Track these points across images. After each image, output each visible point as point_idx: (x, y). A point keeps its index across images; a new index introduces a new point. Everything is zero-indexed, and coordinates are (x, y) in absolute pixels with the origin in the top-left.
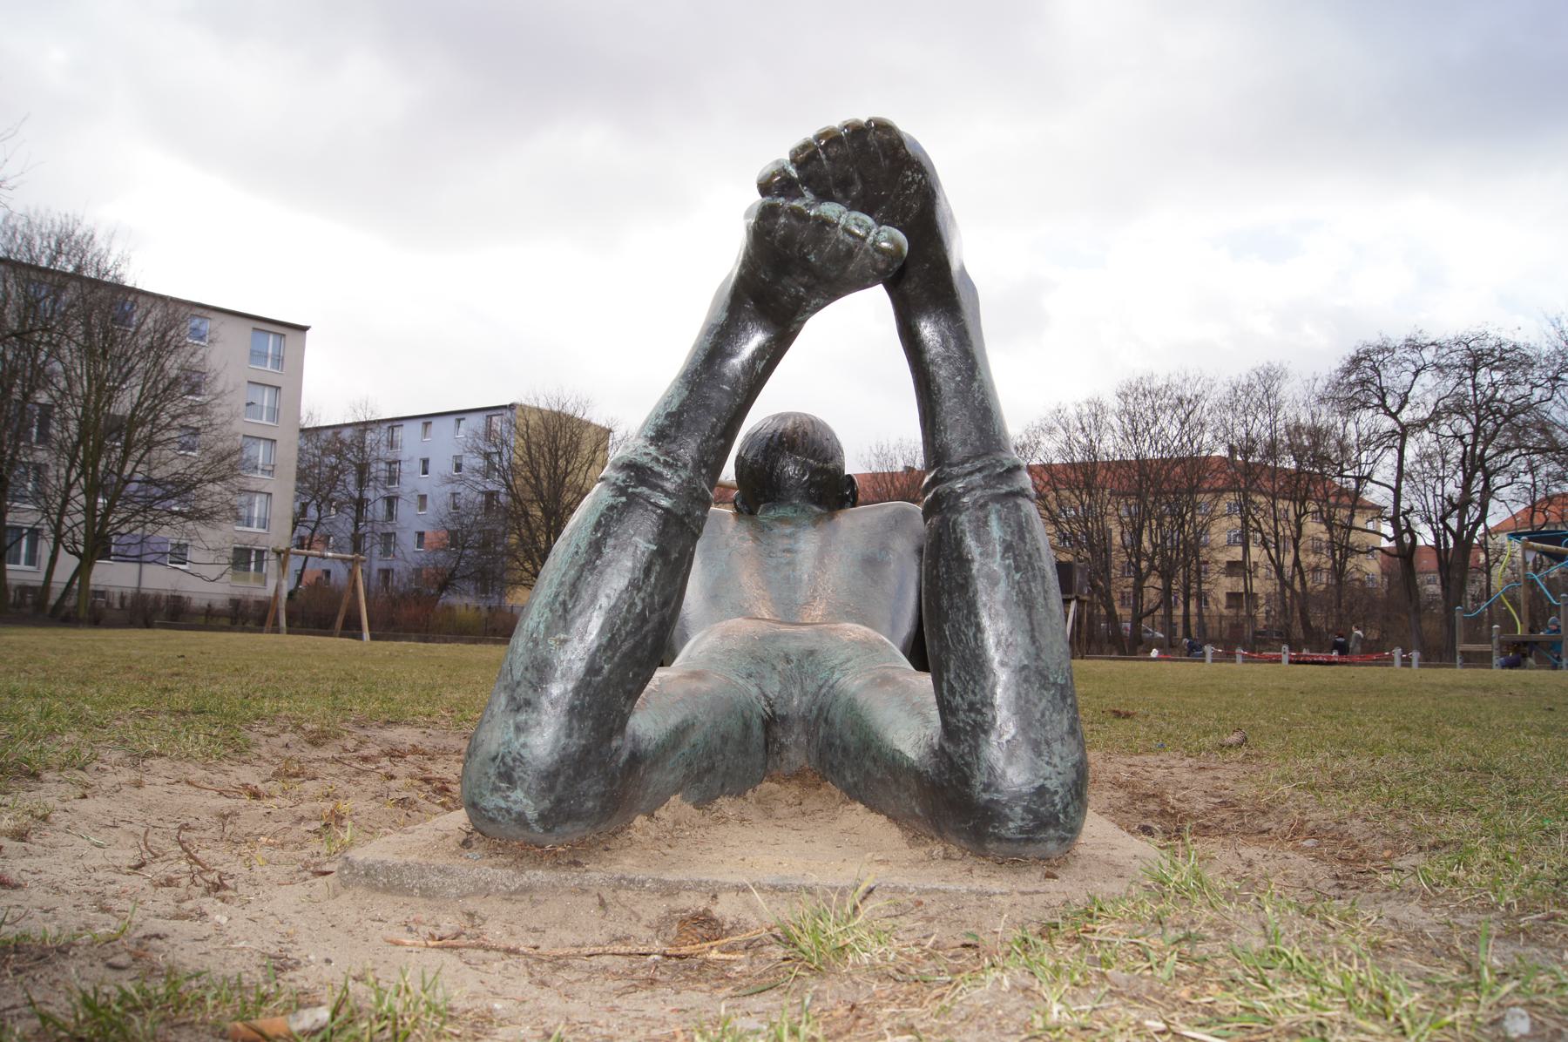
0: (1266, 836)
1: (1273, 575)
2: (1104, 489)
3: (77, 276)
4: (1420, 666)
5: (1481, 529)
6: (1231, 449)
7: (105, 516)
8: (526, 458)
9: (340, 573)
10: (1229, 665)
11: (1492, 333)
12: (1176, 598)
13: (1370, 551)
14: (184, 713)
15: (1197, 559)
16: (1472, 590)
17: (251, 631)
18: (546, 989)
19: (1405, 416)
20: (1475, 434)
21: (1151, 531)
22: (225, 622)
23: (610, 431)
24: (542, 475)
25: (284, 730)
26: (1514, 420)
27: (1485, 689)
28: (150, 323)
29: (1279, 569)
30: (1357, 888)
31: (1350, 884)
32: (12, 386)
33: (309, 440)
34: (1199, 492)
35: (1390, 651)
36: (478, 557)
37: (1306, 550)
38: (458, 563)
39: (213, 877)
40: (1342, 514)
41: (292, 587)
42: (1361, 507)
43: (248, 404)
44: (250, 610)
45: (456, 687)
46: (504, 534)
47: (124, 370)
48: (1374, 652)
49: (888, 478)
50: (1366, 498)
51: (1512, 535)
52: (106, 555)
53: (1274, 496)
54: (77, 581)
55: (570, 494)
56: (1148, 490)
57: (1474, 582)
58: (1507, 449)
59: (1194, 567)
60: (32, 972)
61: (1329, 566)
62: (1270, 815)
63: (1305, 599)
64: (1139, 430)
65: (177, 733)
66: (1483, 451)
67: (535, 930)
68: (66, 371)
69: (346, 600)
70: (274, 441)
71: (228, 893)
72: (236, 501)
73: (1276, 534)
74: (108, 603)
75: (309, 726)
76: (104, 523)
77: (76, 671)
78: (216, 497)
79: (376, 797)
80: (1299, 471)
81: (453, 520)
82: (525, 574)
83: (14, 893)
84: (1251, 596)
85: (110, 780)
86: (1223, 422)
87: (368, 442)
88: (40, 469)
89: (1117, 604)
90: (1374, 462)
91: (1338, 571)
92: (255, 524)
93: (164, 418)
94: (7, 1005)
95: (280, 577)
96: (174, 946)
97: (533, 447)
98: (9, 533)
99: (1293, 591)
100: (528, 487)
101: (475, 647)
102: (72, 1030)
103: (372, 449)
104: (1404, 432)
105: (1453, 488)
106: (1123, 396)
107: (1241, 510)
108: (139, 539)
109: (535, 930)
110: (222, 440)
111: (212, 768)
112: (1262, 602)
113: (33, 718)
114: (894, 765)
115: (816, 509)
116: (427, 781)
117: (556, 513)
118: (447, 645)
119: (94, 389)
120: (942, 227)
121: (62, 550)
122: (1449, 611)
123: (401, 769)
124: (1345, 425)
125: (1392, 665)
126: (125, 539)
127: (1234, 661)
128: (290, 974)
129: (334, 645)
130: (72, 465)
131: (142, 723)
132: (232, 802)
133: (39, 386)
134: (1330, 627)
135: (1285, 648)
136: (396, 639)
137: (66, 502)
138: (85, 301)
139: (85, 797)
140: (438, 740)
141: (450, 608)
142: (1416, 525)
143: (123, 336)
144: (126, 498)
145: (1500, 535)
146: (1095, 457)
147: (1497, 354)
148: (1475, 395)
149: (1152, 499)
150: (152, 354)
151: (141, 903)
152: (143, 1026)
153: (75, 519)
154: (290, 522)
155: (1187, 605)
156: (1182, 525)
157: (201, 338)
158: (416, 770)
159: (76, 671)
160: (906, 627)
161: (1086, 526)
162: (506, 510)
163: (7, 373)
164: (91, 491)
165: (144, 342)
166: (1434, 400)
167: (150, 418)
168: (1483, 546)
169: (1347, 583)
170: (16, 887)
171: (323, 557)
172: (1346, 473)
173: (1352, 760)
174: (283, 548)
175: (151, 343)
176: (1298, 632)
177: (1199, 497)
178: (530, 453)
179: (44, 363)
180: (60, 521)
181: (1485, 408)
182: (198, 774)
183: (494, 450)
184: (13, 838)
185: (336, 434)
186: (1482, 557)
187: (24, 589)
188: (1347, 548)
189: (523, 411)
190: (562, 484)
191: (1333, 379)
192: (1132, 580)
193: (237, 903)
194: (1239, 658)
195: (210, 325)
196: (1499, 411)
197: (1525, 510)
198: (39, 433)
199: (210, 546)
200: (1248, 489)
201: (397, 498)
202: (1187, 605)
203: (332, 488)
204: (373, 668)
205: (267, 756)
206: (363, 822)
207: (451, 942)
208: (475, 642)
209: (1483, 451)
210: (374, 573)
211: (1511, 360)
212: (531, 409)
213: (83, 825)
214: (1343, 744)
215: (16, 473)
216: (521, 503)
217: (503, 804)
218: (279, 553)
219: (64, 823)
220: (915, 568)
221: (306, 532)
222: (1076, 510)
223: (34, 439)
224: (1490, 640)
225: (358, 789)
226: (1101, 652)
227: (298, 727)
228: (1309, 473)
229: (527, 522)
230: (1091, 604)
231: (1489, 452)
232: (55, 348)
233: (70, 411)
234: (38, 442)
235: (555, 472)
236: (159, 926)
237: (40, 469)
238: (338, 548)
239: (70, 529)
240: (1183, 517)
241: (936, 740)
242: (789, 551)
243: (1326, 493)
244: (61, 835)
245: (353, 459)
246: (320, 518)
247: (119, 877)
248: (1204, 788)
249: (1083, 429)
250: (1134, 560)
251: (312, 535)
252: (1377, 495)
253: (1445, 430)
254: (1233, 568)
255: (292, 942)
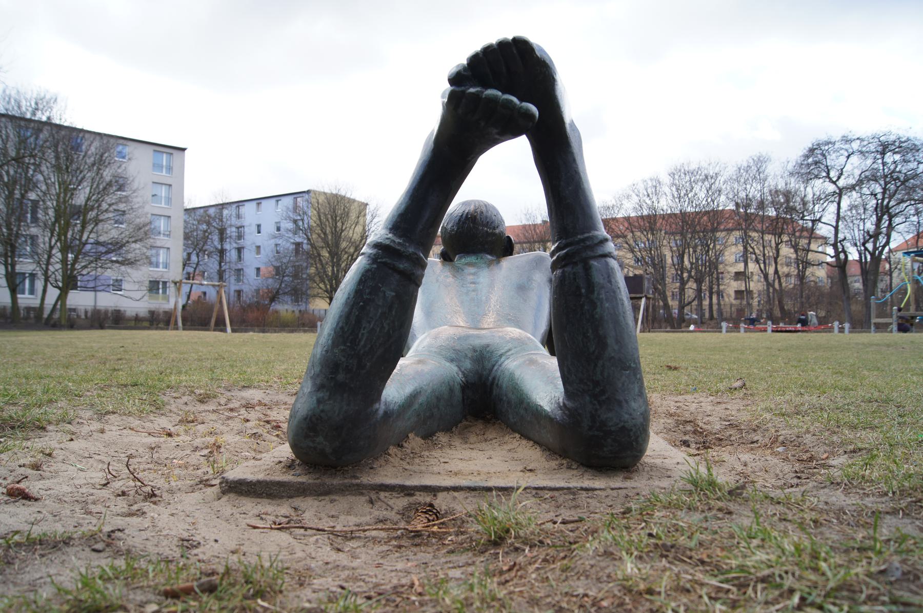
0: (755, 445)
1: (762, 280)
2: (661, 231)
3: (49, 123)
4: (850, 332)
5: (887, 249)
6: (737, 205)
7: (73, 265)
8: (318, 222)
9: (212, 294)
10: (736, 334)
11: (894, 131)
12: (705, 294)
13: (820, 264)
14: (126, 386)
15: (717, 271)
16: (881, 285)
17: (162, 329)
18: (341, 553)
19: (841, 183)
20: (884, 193)
21: (689, 255)
22: (146, 324)
23: (367, 204)
24: (328, 232)
25: (184, 394)
26: (907, 184)
27: (888, 346)
28: (93, 149)
29: (766, 276)
30: (808, 478)
31: (803, 476)
32: (14, 190)
33: (190, 216)
34: (717, 231)
35: (832, 323)
36: (292, 281)
37: (782, 264)
38: (281, 285)
39: (148, 489)
40: (803, 242)
41: (184, 302)
42: (815, 238)
43: (153, 196)
44: (161, 316)
45: (283, 362)
46: (307, 268)
47: (79, 178)
48: (824, 324)
49: (532, 228)
50: (818, 232)
51: (905, 253)
52: (75, 287)
53: (763, 233)
54: (59, 303)
55: (344, 243)
56: (687, 231)
57: (882, 281)
58: (902, 201)
59: (715, 275)
60: (50, 556)
61: (796, 273)
62: (758, 432)
63: (781, 294)
64: (682, 195)
65: (122, 399)
66: (888, 203)
67: (333, 517)
68: (45, 179)
69: (216, 309)
70: (169, 217)
71: (157, 499)
72: (149, 253)
73: (764, 255)
74: (77, 315)
75: (198, 392)
76: (73, 269)
77: (62, 359)
78: (137, 251)
79: (239, 433)
80: (777, 217)
81: (276, 260)
82: (320, 291)
83: (36, 503)
84: (749, 292)
85: (85, 429)
86: (732, 189)
87: (224, 216)
88: (33, 238)
89: (669, 299)
90: (823, 210)
91: (801, 277)
92: (161, 266)
93: (104, 206)
94: (38, 577)
95: (177, 297)
96: (128, 535)
97: (322, 215)
98: (18, 277)
99: (774, 289)
100: (320, 240)
101: (292, 335)
102: (75, 594)
103: (227, 220)
104: (840, 193)
105: (870, 226)
106: (672, 175)
107: (743, 241)
108: (93, 278)
109: (333, 517)
110: (139, 217)
111: (144, 419)
112: (755, 295)
113: (39, 393)
114: (537, 413)
115: (489, 257)
116: (268, 422)
117: (337, 254)
118: (276, 334)
119: (62, 190)
120: (559, 97)
121: (49, 285)
122: (867, 299)
123: (253, 415)
124: (805, 188)
125: (833, 332)
126: (86, 278)
127: (739, 332)
128: (195, 551)
129: (210, 336)
130: (52, 235)
131: (102, 393)
132: (157, 439)
133: (30, 190)
134: (796, 309)
135: (769, 323)
136: (246, 331)
137: (50, 257)
138: (54, 138)
139: (72, 440)
140: (273, 397)
141: (277, 312)
142: (848, 248)
143: (78, 158)
144: (84, 254)
145: (898, 253)
146: (655, 212)
147: (897, 144)
148: (884, 169)
149: (690, 236)
150: (95, 168)
151: (108, 507)
152: (114, 590)
153: (56, 267)
154: (182, 264)
155: (711, 298)
156: (708, 251)
157: (124, 157)
158: (262, 416)
159: (62, 359)
160: (543, 326)
161: (651, 254)
162: (308, 253)
163: (11, 182)
164: (65, 250)
165: (90, 161)
166: (860, 173)
167: (96, 205)
168: (888, 259)
169: (806, 283)
170: (36, 500)
171: (202, 285)
172: (806, 218)
173: (806, 397)
174: (178, 280)
175: (95, 161)
176: (777, 313)
177: (718, 234)
178: (320, 219)
179: (32, 175)
180: (47, 269)
181: (890, 177)
182: (135, 423)
183: (299, 218)
184: (33, 469)
185: (205, 212)
186: (887, 266)
187: (28, 309)
188: (807, 263)
189: (315, 194)
190: (340, 237)
191: (799, 162)
192: (678, 284)
193: (162, 504)
194: (742, 330)
195: (129, 149)
196: (898, 178)
197: (913, 237)
198: (32, 217)
199: (136, 280)
200: (747, 228)
201: (243, 248)
202: (711, 298)
203: (205, 243)
204: (234, 350)
205: (175, 410)
206: (232, 449)
207: (285, 526)
208: (292, 331)
209: (888, 203)
210: (232, 293)
211: (906, 148)
212: (320, 193)
213: (72, 457)
214: (802, 386)
215: (20, 241)
216: (316, 248)
217: (311, 445)
218: (175, 283)
219: (61, 458)
220: (548, 291)
221: (191, 270)
222: (645, 244)
223: (29, 221)
224: (891, 317)
225: (228, 429)
226: (660, 328)
227: (192, 392)
228: (784, 218)
229: (320, 260)
230: (654, 299)
231: (892, 203)
232: (37, 166)
233: (49, 203)
234: (32, 222)
235: (335, 230)
236: (120, 522)
237: (33, 238)
238: (210, 278)
239: (53, 273)
240: (708, 246)
241: (561, 400)
242: (474, 283)
243: (794, 230)
244: (60, 465)
245: (216, 226)
246: (198, 262)
247: (95, 491)
248: (720, 415)
249: (648, 196)
250: (679, 272)
251: (195, 271)
252: (824, 230)
253: (865, 191)
254: (738, 275)
255: (195, 528)
